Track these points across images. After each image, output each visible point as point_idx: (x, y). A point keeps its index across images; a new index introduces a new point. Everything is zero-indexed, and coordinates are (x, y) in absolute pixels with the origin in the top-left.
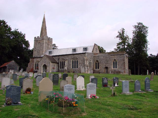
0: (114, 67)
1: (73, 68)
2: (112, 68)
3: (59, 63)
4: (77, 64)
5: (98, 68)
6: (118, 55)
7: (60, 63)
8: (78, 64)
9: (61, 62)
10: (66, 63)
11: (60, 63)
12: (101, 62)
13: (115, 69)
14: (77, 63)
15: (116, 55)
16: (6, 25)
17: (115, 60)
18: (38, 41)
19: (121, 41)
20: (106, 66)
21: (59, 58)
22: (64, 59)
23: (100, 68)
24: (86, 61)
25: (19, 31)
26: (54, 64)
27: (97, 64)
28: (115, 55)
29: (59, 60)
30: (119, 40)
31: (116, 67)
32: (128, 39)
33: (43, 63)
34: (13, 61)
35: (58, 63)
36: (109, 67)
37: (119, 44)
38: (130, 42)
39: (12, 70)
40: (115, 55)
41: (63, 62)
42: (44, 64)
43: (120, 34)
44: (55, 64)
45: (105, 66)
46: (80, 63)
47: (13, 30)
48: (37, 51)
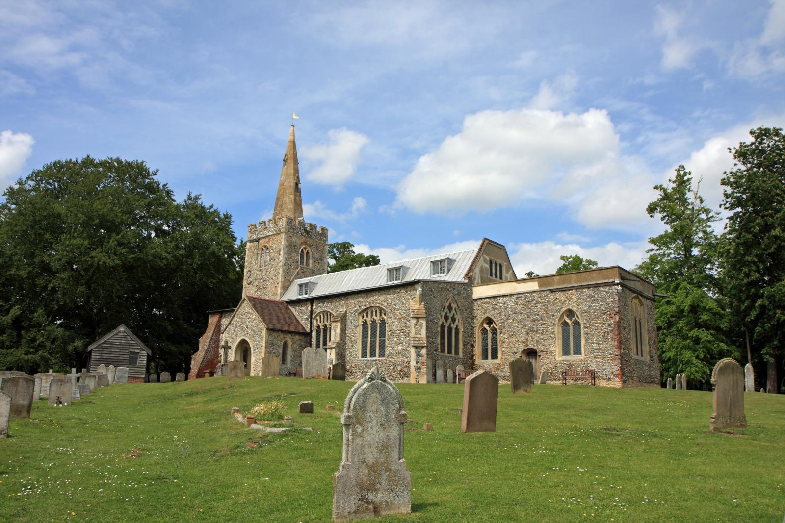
0: (566, 352)
1: (364, 355)
2: (559, 357)
3: (311, 331)
4: (380, 337)
5: (495, 356)
6: (582, 287)
7: (314, 334)
8: (387, 334)
9: (319, 327)
10: (335, 331)
11: (314, 334)
12: (504, 327)
13: (572, 358)
14: (382, 334)
15: (577, 288)
16: (147, 181)
17: (570, 313)
18: (260, 241)
19: (669, 229)
20: (531, 346)
21: (312, 312)
22: (331, 314)
23: (500, 355)
24: (414, 321)
25: (206, 202)
26: (282, 336)
27: (571, 328)
28: (571, 288)
29: (311, 318)
30: (660, 226)
31: (578, 351)
32: (703, 216)
33: (237, 335)
34: (122, 329)
35: (309, 335)
36: (543, 348)
37: (662, 241)
38: (719, 228)
39: (107, 366)
40: (571, 288)
41: (374, 321)
42: (239, 340)
43: (666, 197)
44: (288, 338)
45: (522, 347)
46: (393, 333)
47: (180, 198)
48: (256, 283)
